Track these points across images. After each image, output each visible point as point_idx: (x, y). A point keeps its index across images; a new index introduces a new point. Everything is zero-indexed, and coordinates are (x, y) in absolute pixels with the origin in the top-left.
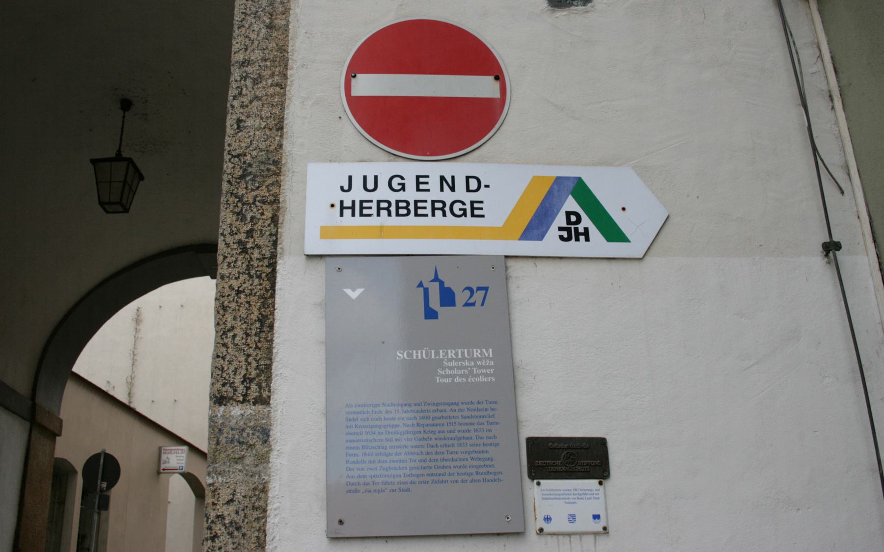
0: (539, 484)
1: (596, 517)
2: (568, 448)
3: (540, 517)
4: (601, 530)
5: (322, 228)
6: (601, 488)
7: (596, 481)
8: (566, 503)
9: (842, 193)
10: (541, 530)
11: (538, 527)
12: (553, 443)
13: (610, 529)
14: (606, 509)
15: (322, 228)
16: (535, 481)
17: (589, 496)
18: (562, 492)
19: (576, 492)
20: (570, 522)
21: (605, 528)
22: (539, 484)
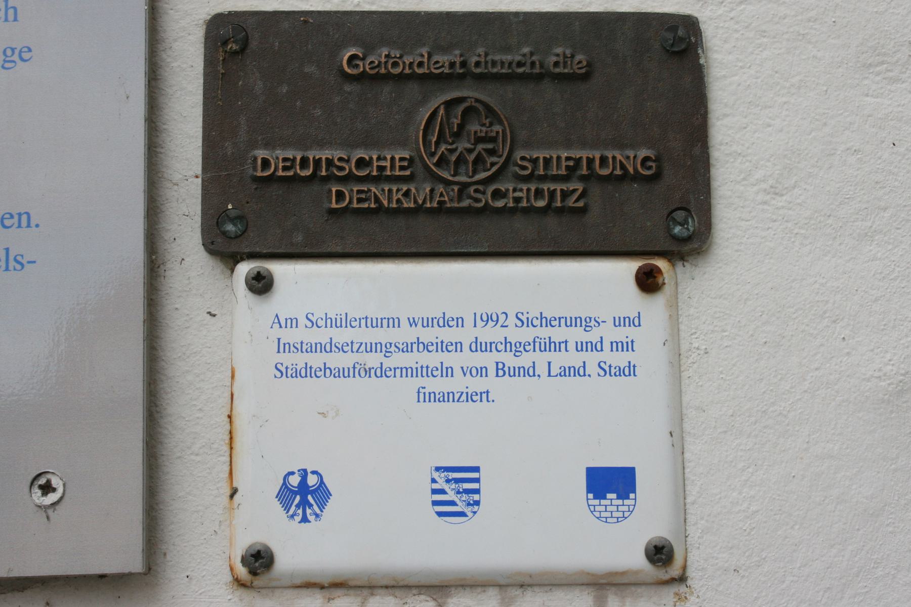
0: (261, 285)
1: (611, 482)
2: (460, 75)
3: (260, 482)
4: (637, 560)
5: (632, 470)
6: (654, 309)
7: (628, 268)
8: (425, 396)
9: (475, 326)
10: (259, 560)
11: (243, 542)
12: (369, 48)
13: (700, 556)
14: (677, 437)
15: (632, 470)
16: (244, 268)
17: (573, 359)
18: (406, 334)
19: (490, 334)
20: (445, 510)
21: (659, 553)
22: (261, 285)
